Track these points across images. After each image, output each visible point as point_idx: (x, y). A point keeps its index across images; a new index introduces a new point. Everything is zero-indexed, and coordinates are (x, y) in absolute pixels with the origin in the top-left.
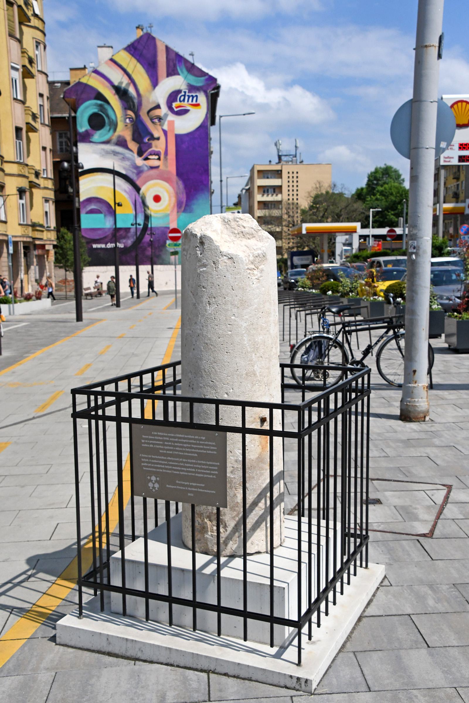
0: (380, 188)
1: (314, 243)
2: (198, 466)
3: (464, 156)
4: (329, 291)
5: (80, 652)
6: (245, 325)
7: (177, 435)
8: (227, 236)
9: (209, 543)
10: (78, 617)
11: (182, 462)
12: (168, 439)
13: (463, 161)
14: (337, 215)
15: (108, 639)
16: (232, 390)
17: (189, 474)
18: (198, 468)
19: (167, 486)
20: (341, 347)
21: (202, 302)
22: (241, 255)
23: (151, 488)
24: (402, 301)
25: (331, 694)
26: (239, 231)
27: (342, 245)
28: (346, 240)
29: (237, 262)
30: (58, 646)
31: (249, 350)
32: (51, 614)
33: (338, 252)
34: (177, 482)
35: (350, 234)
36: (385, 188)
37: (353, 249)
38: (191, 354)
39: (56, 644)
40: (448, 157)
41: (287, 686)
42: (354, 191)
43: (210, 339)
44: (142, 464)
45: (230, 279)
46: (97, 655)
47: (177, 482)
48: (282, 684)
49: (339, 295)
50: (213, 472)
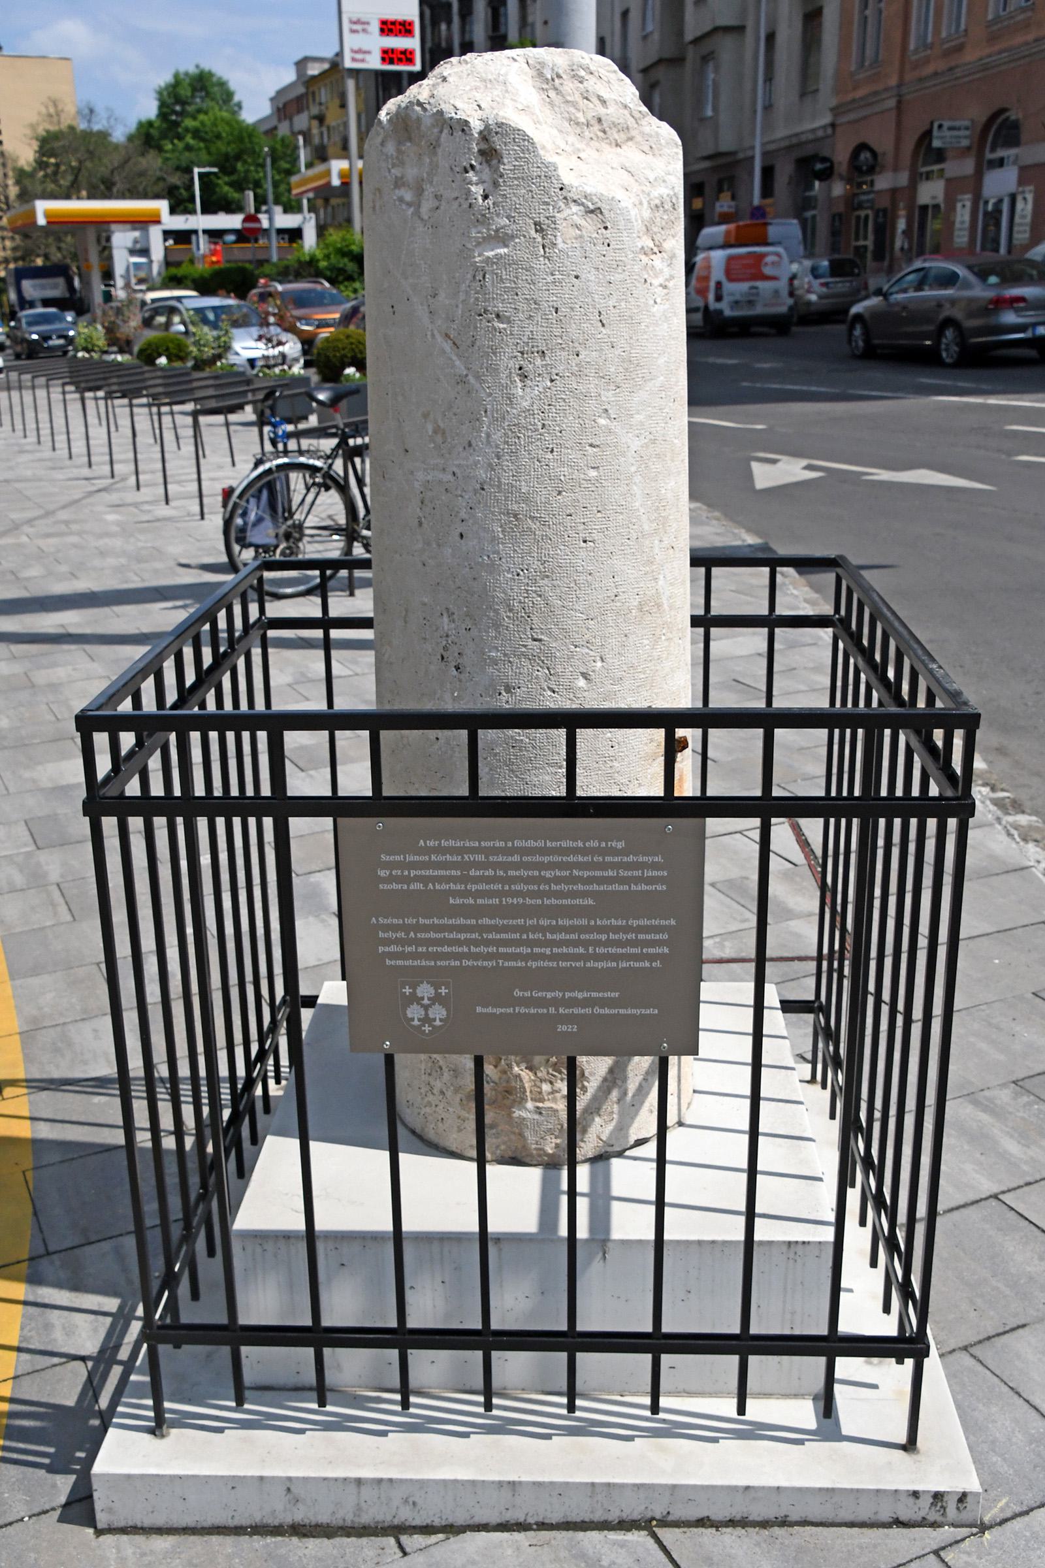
0: (189, 123)
1: (59, 249)
2: (595, 936)
3: (393, 51)
4: (160, 355)
5: (195, 1543)
6: (636, 444)
7: (517, 843)
8: (555, 132)
9: (527, 1134)
10: (152, 1431)
11: (536, 929)
12: (481, 858)
13: (391, 62)
14: (103, 182)
15: (289, 1489)
16: (599, 664)
17: (563, 964)
18: (598, 943)
19: (479, 1009)
20: (343, 489)
21: (494, 370)
22: (626, 201)
23: (416, 1023)
24: (358, 375)
25: (1027, 1513)
26: (590, 115)
27: (126, 253)
28: (136, 241)
29: (614, 223)
30: (108, 1539)
31: (646, 527)
32: (11, 1415)
33: (119, 269)
34: (518, 993)
35: (141, 229)
36: (202, 123)
37: (151, 262)
38: (448, 551)
39: (99, 1533)
40: (359, 51)
41: (903, 1518)
42: (132, 127)
43: (526, 499)
44: (381, 949)
45: (593, 287)
46: (258, 1542)
47: (518, 993)
48: (885, 1516)
49: (190, 364)
50: (651, 950)
